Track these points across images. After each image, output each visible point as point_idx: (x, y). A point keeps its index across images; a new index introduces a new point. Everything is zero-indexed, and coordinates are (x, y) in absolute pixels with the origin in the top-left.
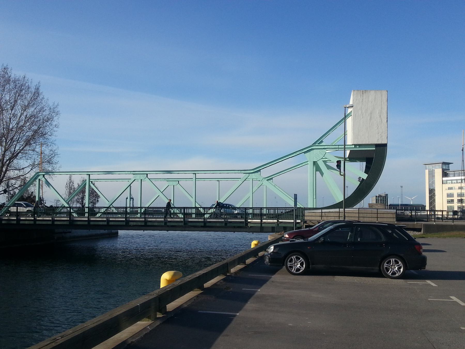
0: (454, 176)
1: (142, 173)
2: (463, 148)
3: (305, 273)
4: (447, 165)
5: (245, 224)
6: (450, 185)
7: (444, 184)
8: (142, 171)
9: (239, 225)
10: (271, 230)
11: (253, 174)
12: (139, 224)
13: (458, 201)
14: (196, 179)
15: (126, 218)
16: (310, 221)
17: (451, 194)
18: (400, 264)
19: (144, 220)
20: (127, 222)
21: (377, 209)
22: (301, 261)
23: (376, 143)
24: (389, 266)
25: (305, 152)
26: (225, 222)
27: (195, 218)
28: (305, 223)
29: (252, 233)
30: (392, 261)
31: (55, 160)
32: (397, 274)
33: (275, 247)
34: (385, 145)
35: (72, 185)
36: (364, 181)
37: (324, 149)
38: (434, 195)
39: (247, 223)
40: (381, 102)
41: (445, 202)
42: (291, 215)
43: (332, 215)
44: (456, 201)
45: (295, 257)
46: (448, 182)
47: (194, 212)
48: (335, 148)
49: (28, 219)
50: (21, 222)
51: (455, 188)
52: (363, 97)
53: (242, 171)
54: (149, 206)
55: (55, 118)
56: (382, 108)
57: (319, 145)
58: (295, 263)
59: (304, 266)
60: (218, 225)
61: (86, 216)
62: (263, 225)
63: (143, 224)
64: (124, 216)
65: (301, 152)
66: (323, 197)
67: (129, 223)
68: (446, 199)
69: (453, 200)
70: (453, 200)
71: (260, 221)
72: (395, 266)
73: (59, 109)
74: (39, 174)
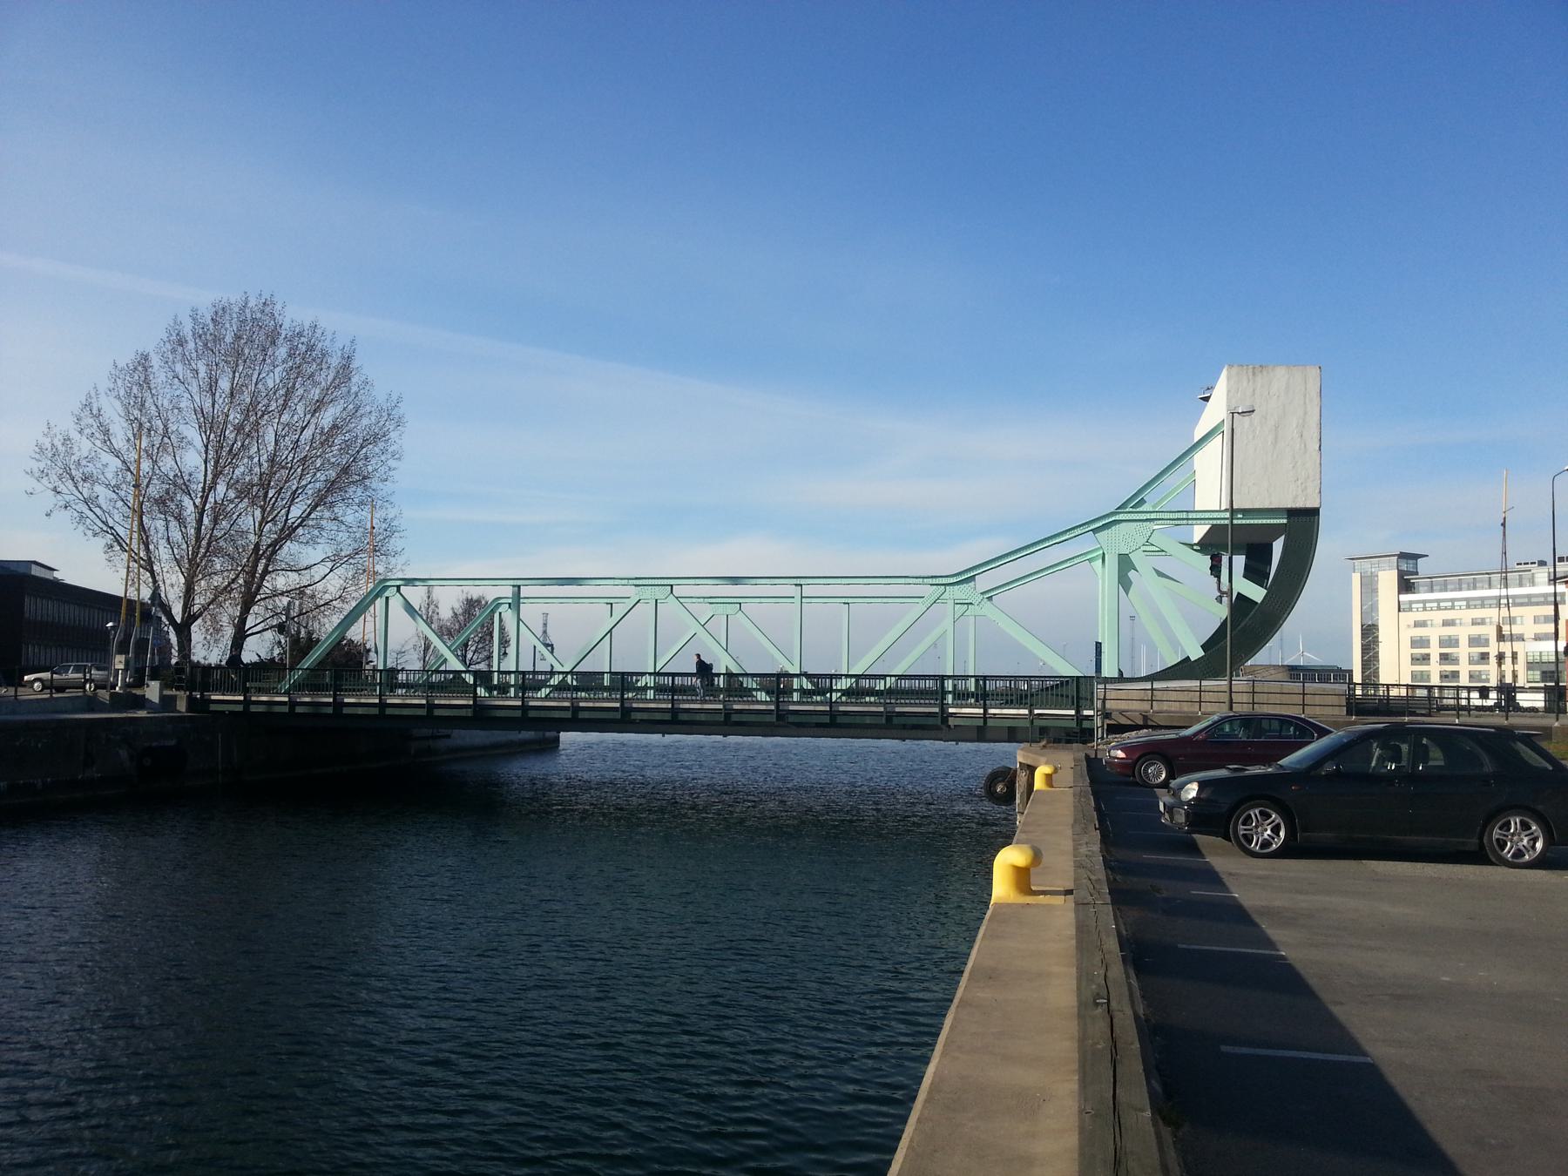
0: (1432, 591)
1: (659, 582)
2: (1505, 518)
3: (1285, 852)
4: (1411, 562)
5: (940, 718)
6: (1421, 616)
7: (1404, 611)
8: (658, 578)
9: (914, 721)
10: (1006, 736)
11: (956, 587)
12: (658, 716)
13: (1441, 659)
14: (802, 597)
15: (622, 700)
16: (1121, 712)
17: (1452, 638)
18: (1535, 831)
19: (670, 706)
20: (626, 711)
21: (1254, 681)
22: (1273, 821)
23: (1289, 506)
24: (1252, 830)
25: (1095, 531)
26: (887, 712)
27: (798, 703)
28: (1107, 718)
29: (954, 743)
30: (1253, 816)
31: (395, 543)
32: (1527, 857)
33: (1203, 785)
34: (1314, 513)
35: (433, 612)
36: (1257, 606)
37: (1147, 520)
38: (1376, 641)
39: (945, 716)
40: (1305, 396)
41: (1406, 660)
42: (1057, 695)
43: (1173, 696)
44: (1435, 658)
45: (1257, 811)
46: (1414, 606)
47: (652, 685)
48: (1178, 519)
49: (363, 701)
50: (346, 711)
51: (1434, 622)
52: (1254, 381)
53: (925, 580)
54: (573, 668)
55: (393, 435)
56: (1305, 413)
57: (1134, 510)
58: (1256, 827)
59: (1282, 834)
60: (868, 720)
61: (648, 697)
62: (990, 723)
63: (667, 717)
64: (618, 696)
65: (1087, 530)
66: (1065, 646)
67: (630, 715)
68: (1407, 651)
69: (1428, 655)
70: (1428, 655)
71: (981, 711)
72: (1522, 836)
73: (403, 409)
74: (388, 584)
